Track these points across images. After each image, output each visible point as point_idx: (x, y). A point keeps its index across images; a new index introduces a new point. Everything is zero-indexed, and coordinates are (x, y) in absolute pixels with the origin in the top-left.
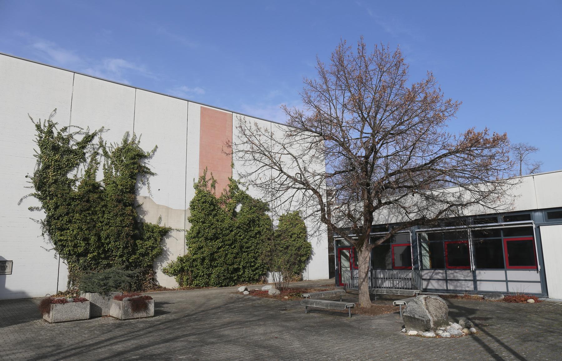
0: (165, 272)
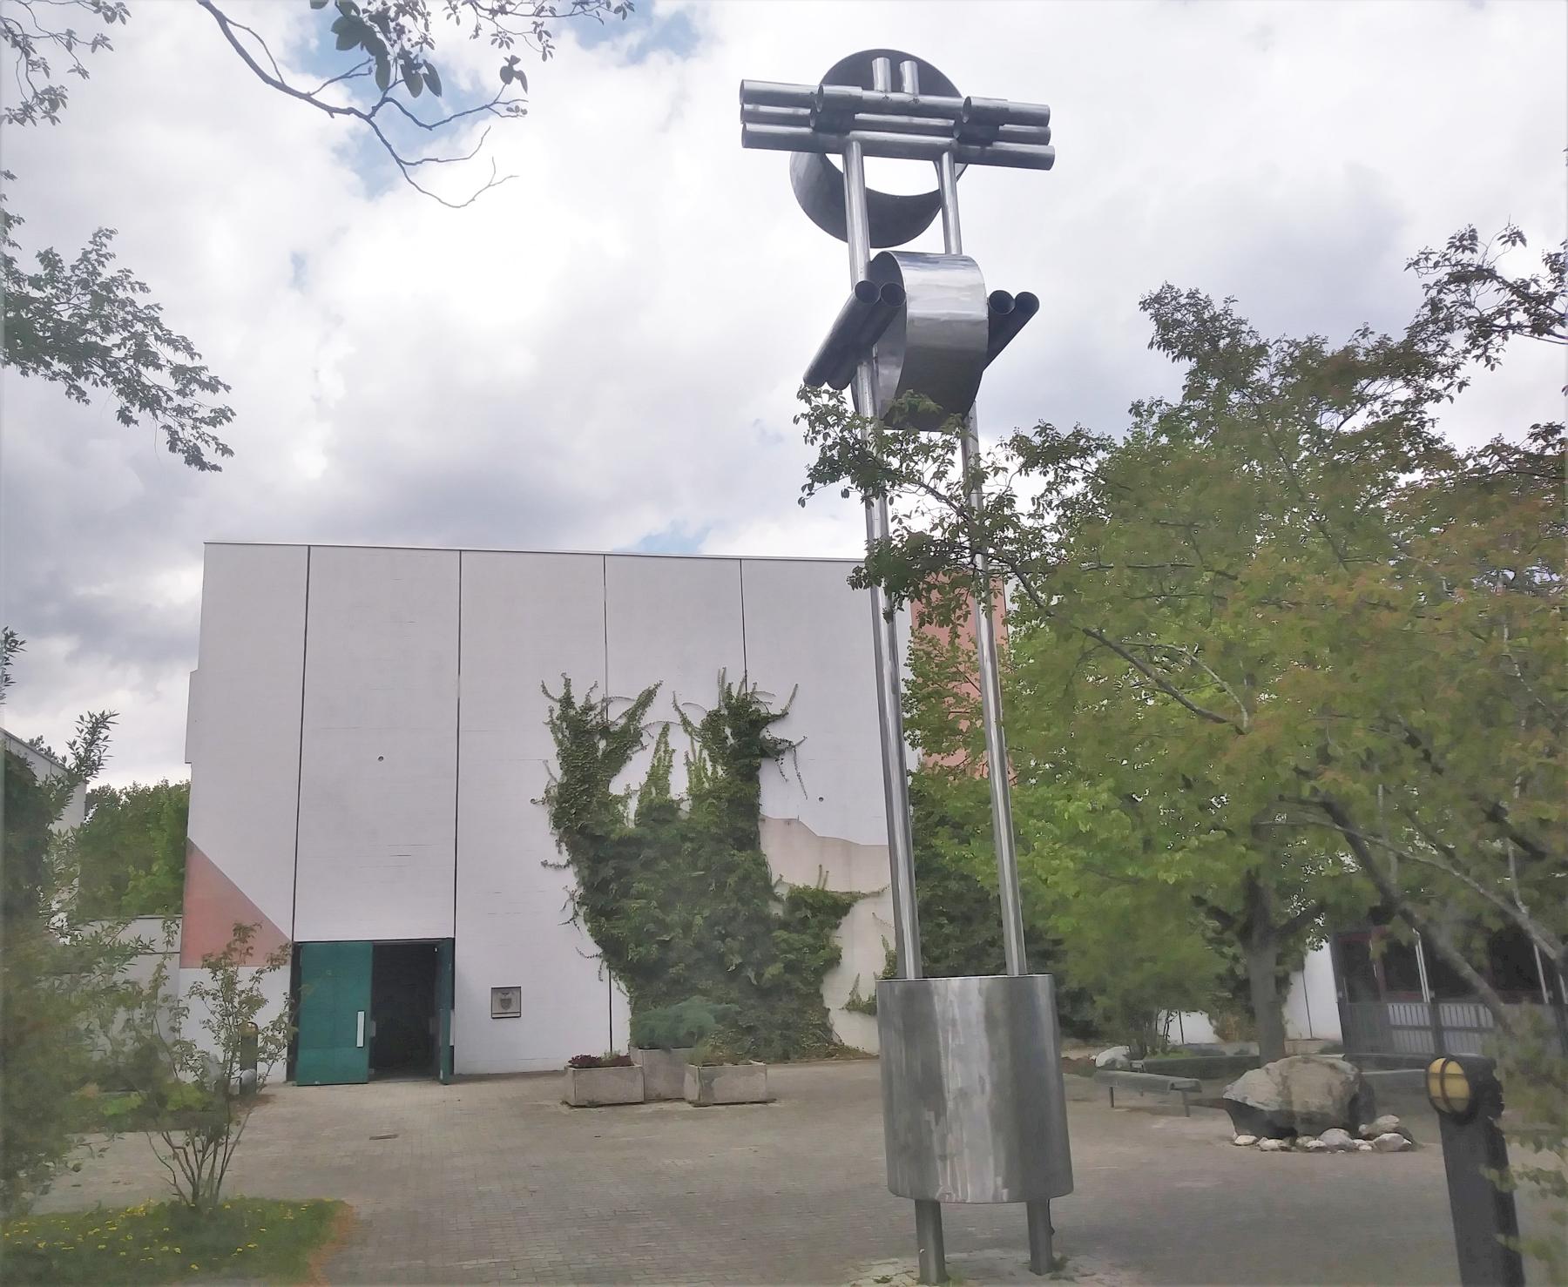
0: (853, 1006)
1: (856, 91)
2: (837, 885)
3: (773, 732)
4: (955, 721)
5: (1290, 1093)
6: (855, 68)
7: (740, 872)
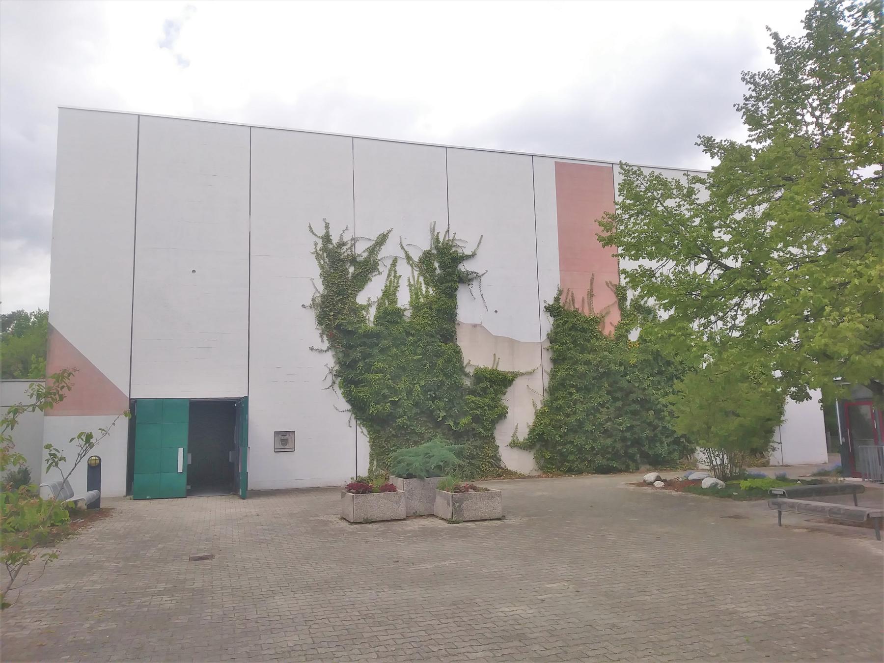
0: (514, 445)
3: (465, 267)
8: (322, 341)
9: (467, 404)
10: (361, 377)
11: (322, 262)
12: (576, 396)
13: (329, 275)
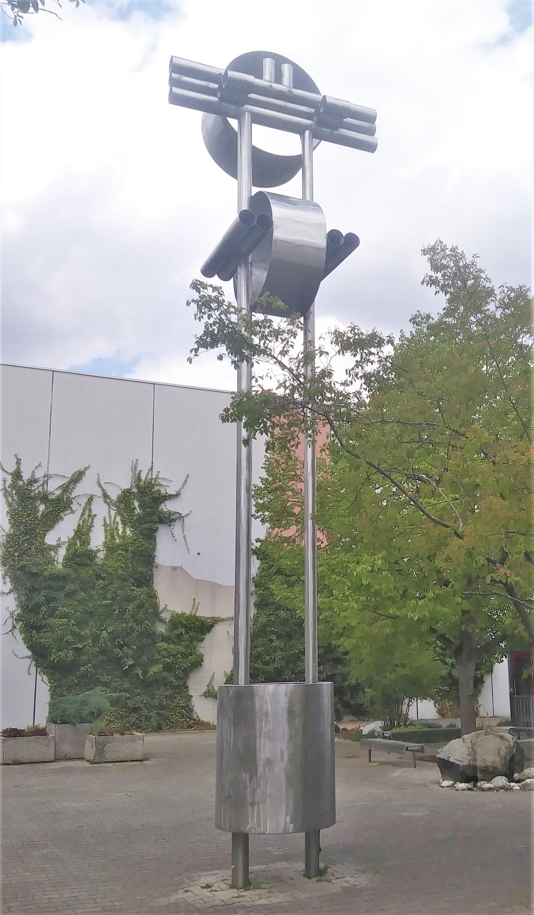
0: (209, 694)
1: (250, 78)
2: (204, 612)
3: (168, 506)
4: (292, 507)
5: (475, 754)
6: (251, 62)
7: (137, 602)
8: (5, 583)
9: (159, 652)
10: (43, 622)
11: (10, 499)
12: (276, 644)
13: (16, 514)
